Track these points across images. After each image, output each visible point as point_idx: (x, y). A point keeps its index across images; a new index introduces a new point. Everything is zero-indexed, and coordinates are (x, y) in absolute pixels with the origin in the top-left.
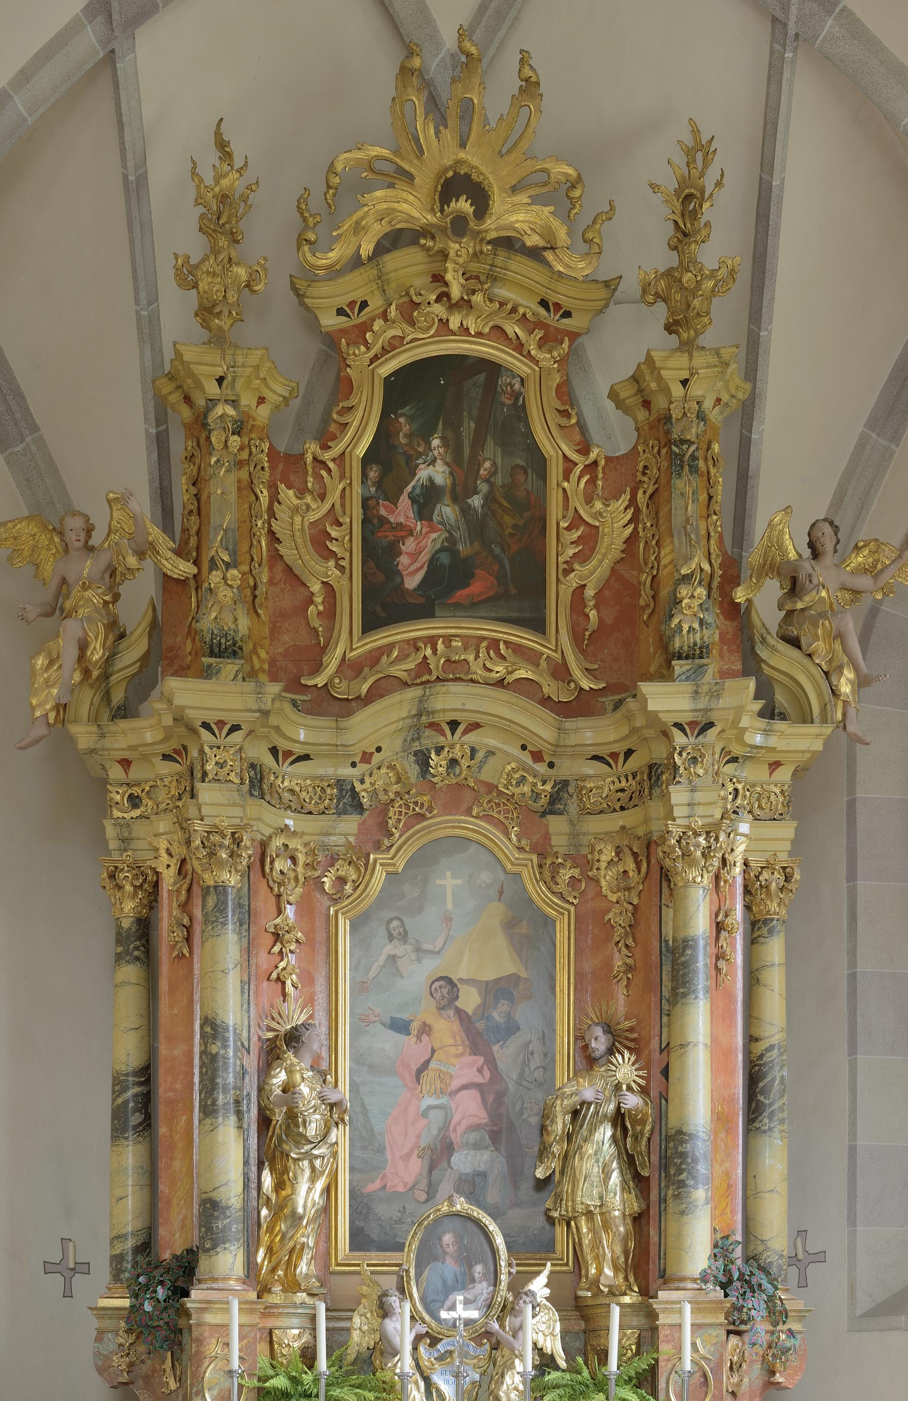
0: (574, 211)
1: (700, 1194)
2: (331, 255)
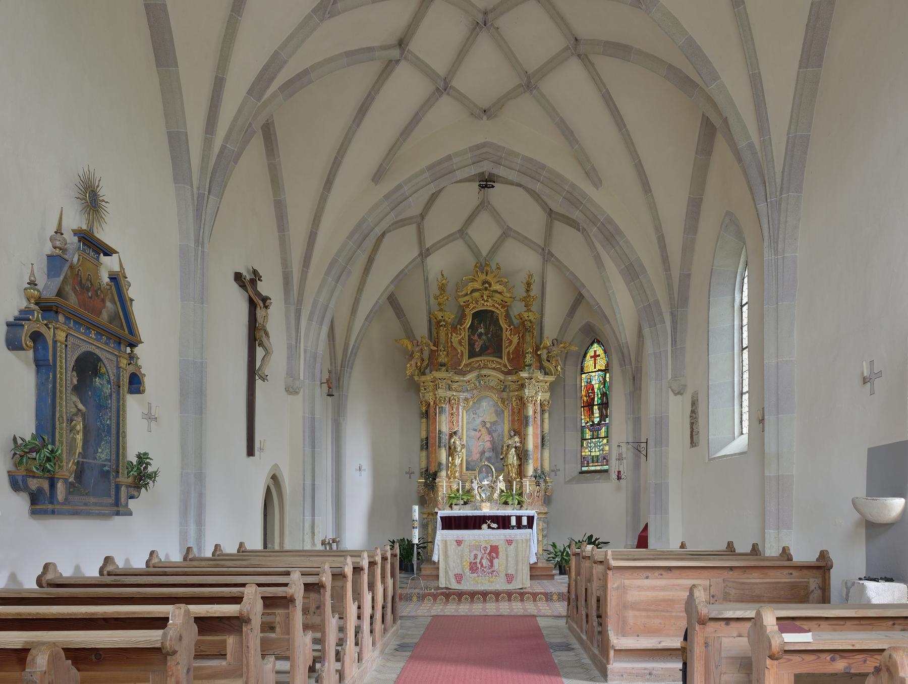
1: (530, 461)
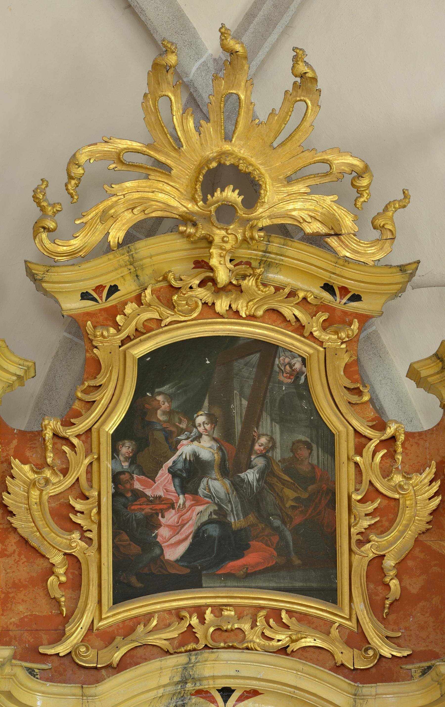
0: (362, 200)
2: (73, 242)
